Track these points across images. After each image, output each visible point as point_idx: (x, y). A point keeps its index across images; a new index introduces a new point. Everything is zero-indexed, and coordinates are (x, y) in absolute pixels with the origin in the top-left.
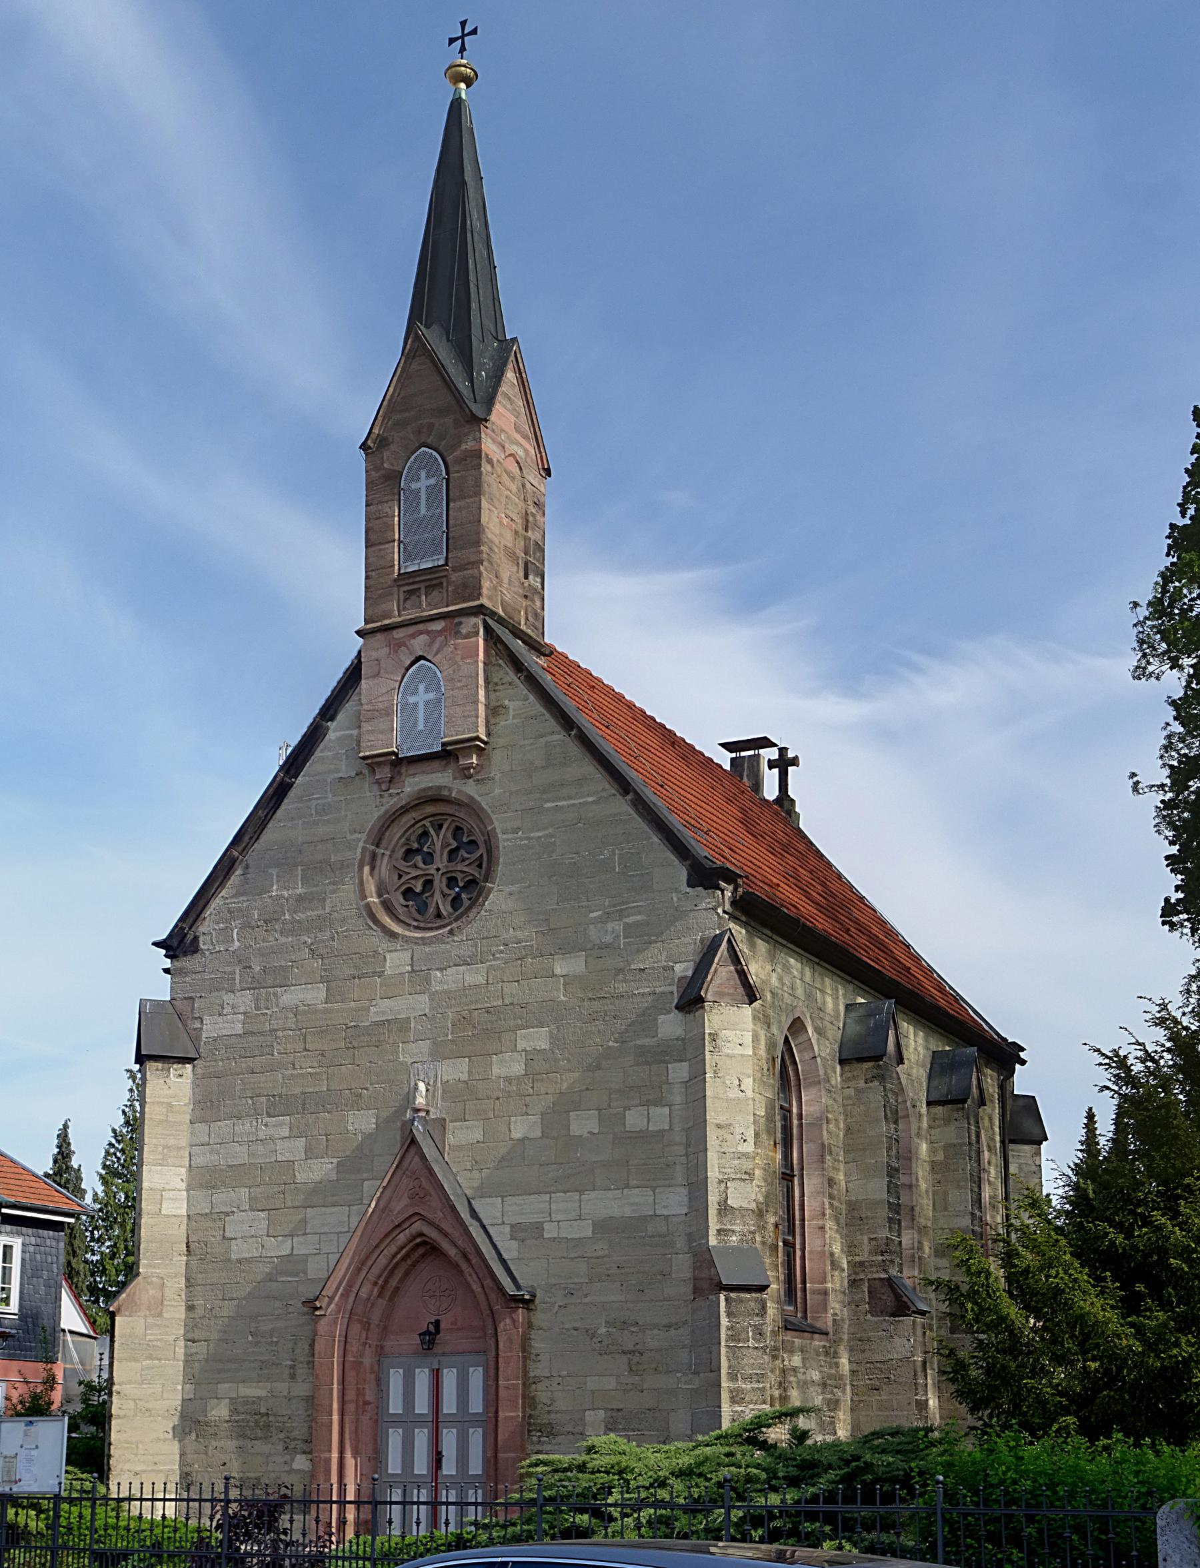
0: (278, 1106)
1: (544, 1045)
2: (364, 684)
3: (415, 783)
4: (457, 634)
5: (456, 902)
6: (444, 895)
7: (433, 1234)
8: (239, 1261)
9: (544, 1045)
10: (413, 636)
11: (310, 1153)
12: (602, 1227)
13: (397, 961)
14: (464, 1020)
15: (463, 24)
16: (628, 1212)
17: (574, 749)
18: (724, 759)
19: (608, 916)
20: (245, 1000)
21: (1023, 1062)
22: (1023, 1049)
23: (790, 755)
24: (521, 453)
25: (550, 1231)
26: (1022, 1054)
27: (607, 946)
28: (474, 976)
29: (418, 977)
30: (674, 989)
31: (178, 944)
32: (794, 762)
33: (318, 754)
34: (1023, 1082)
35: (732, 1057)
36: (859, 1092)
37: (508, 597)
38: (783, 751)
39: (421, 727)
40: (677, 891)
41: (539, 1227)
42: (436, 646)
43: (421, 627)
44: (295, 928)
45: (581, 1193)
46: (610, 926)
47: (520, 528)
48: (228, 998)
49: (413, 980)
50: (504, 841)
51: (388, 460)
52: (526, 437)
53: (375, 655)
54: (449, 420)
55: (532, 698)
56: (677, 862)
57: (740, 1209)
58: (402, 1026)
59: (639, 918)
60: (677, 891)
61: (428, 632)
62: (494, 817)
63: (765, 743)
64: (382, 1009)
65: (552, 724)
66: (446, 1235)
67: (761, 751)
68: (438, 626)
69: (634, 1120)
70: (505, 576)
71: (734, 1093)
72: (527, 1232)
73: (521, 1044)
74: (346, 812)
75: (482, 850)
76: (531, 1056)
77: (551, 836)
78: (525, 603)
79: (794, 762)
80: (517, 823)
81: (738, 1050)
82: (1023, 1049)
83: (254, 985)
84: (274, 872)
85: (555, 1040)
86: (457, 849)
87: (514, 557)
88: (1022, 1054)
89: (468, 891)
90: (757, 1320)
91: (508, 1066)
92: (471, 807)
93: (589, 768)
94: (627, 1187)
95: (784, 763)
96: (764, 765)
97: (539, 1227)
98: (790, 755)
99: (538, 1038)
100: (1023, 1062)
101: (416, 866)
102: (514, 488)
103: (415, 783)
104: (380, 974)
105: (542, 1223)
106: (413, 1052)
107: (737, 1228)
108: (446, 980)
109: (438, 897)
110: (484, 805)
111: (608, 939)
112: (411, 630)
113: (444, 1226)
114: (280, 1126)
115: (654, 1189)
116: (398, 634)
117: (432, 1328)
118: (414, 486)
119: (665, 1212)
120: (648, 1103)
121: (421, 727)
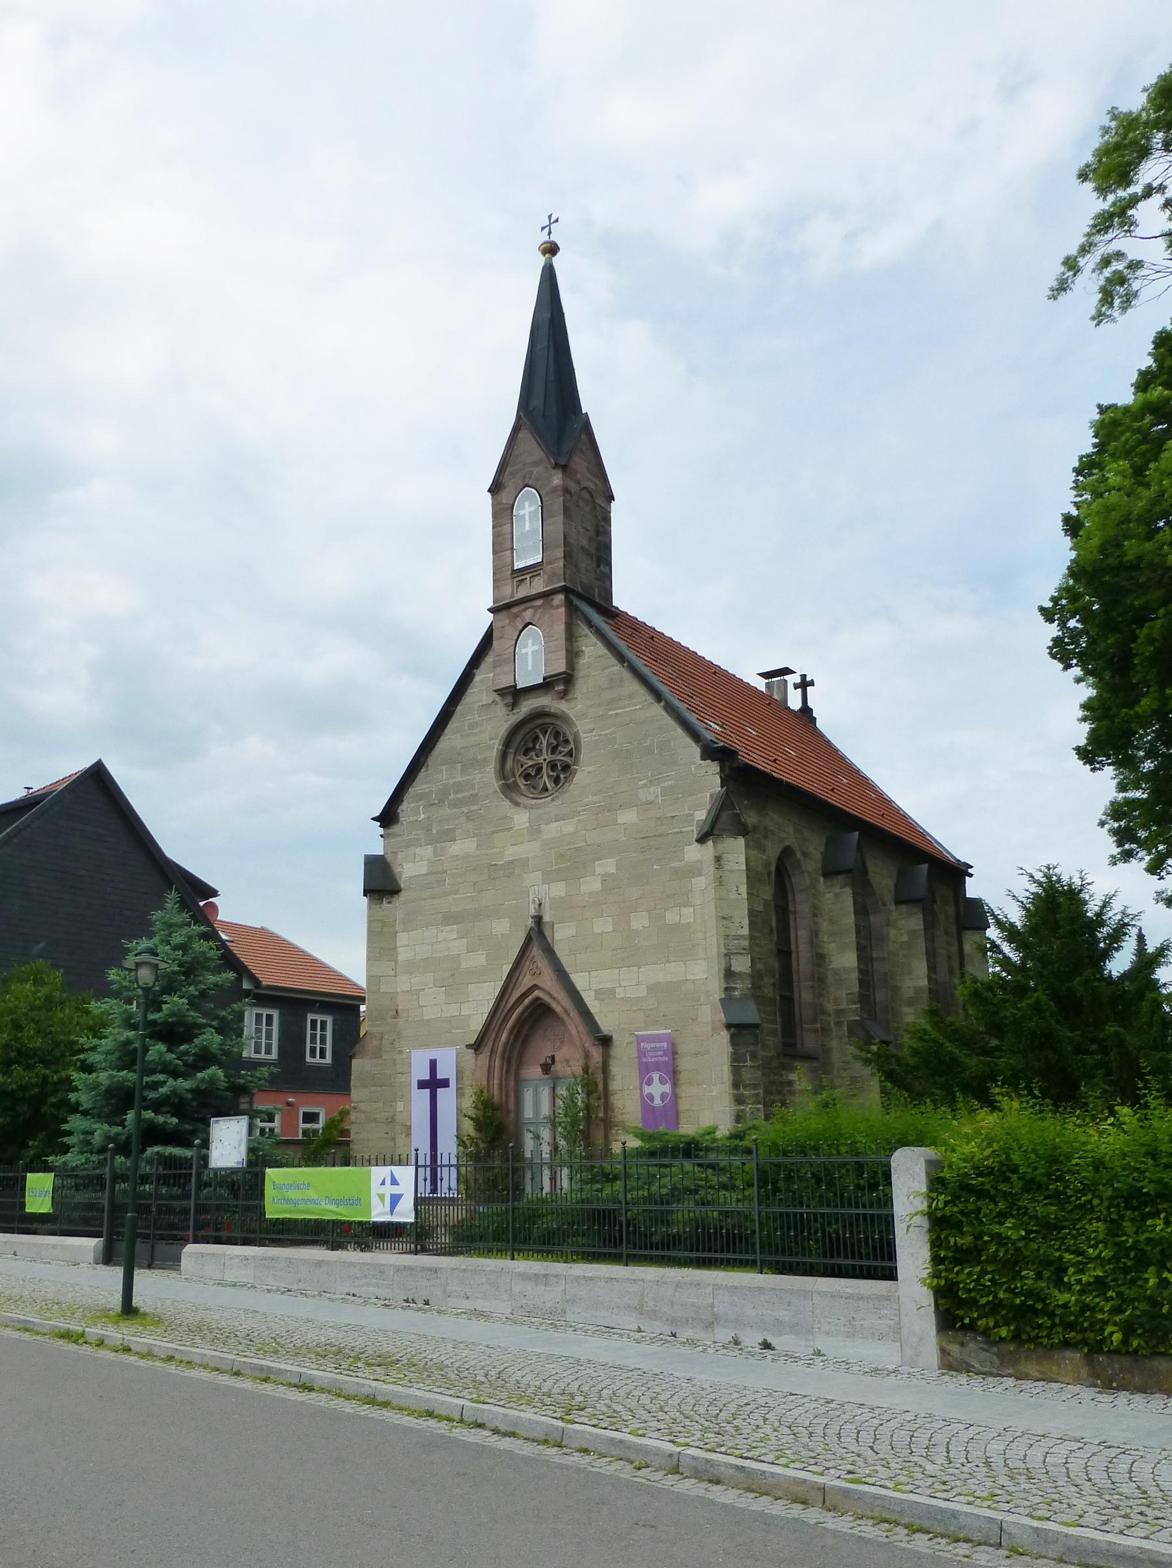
0: (449, 919)
1: (612, 870)
2: (495, 643)
3: (528, 706)
4: (552, 607)
5: (556, 780)
6: (549, 776)
7: (546, 998)
8: (428, 1021)
9: (612, 870)
10: (524, 610)
11: (470, 949)
12: (653, 989)
13: (521, 818)
14: (561, 857)
15: (550, 217)
16: (669, 978)
17: (627, 674)
18: (761, 684)
19: (651, 783)
20: (427, 851)
21: (971, 875)
22: (971, 867)
23: (808, 679)
24: (592, 486)
25: (620, 992)
26: (970, 871)
27: (651, 803)
28: (568, 827)
29: (534, 830)
30: (694, 828)
31: (387, 818)
32: (812, 683)
33: (469, 691)
34: (973, 889)
35: (731, 871)
36: (836, 895)
37: (585, 579)
38: (804, 677)
39: (530, 668)
40: (694, 763)
41: (613, 991)
42: (538, 616)
43: (528, 604)
44: (456, 804)
45: (639, 967)
46: (652, 789)
47: (593, 534)
48: (418, 850)
49: (530, 831)
50: (585, 738)
51: (505, 496)
52: (594, 475)
53: (501, 624)
54: (541, 468)
55: (599, 644)
56: (693, 744)
57: (740, 974)
58: (524, 863)
59: (670, 783)
60: (694, 763)
61: (532, 607)
62: (578, 723)
63: (787, 671)
64: (513, 852)
65: (612, 660)
66: (554, 999)
67: (786, 677)
68: (539, 602)
69: (671, 917)
70: (583, 566)
71: (733, 896)
72: (604, 994)
73: (599, 870)
74: (486, 726)
75: (572, 745)
76: (605, 878)
77: (614, 732)
78: (598, 583)
79: (812, 683)
80: (591, 727)
81: (736, 867)
82: (971, 867)
83: (432, 841)
84: (444, 768)
85: (619, 866)
86: (557, 746)
87: (589, 554)
88: (970, 871)
89: (562, 771)
90: (752, 1048)
91: (591, 885)
92: (564, 718)
93: (635, 687)
94: (668, 962)
95: (804, 684)
96: (790, 687)
97: (613, 991)
98: (808, 679)
99: (608, 866)
100: (971, 875)
101: (531, 759)
102: (587, 509)
103: (528, 706)
104: (509, 829)
105: (614, 988)
106: (533, 878)
107: (738, 986)
108: (551, 830)
109: (545, 777)
110: (571, 716)
111: (651, 798)
112: (522, 607)
113: (553, 993)
114: (450, 933)
115: (684, 962)
116: (515, 610)
117: (549, 1061)
118: (521, 513)
119: (693, 978)
120: (680, 905)
121: (530, 668)
